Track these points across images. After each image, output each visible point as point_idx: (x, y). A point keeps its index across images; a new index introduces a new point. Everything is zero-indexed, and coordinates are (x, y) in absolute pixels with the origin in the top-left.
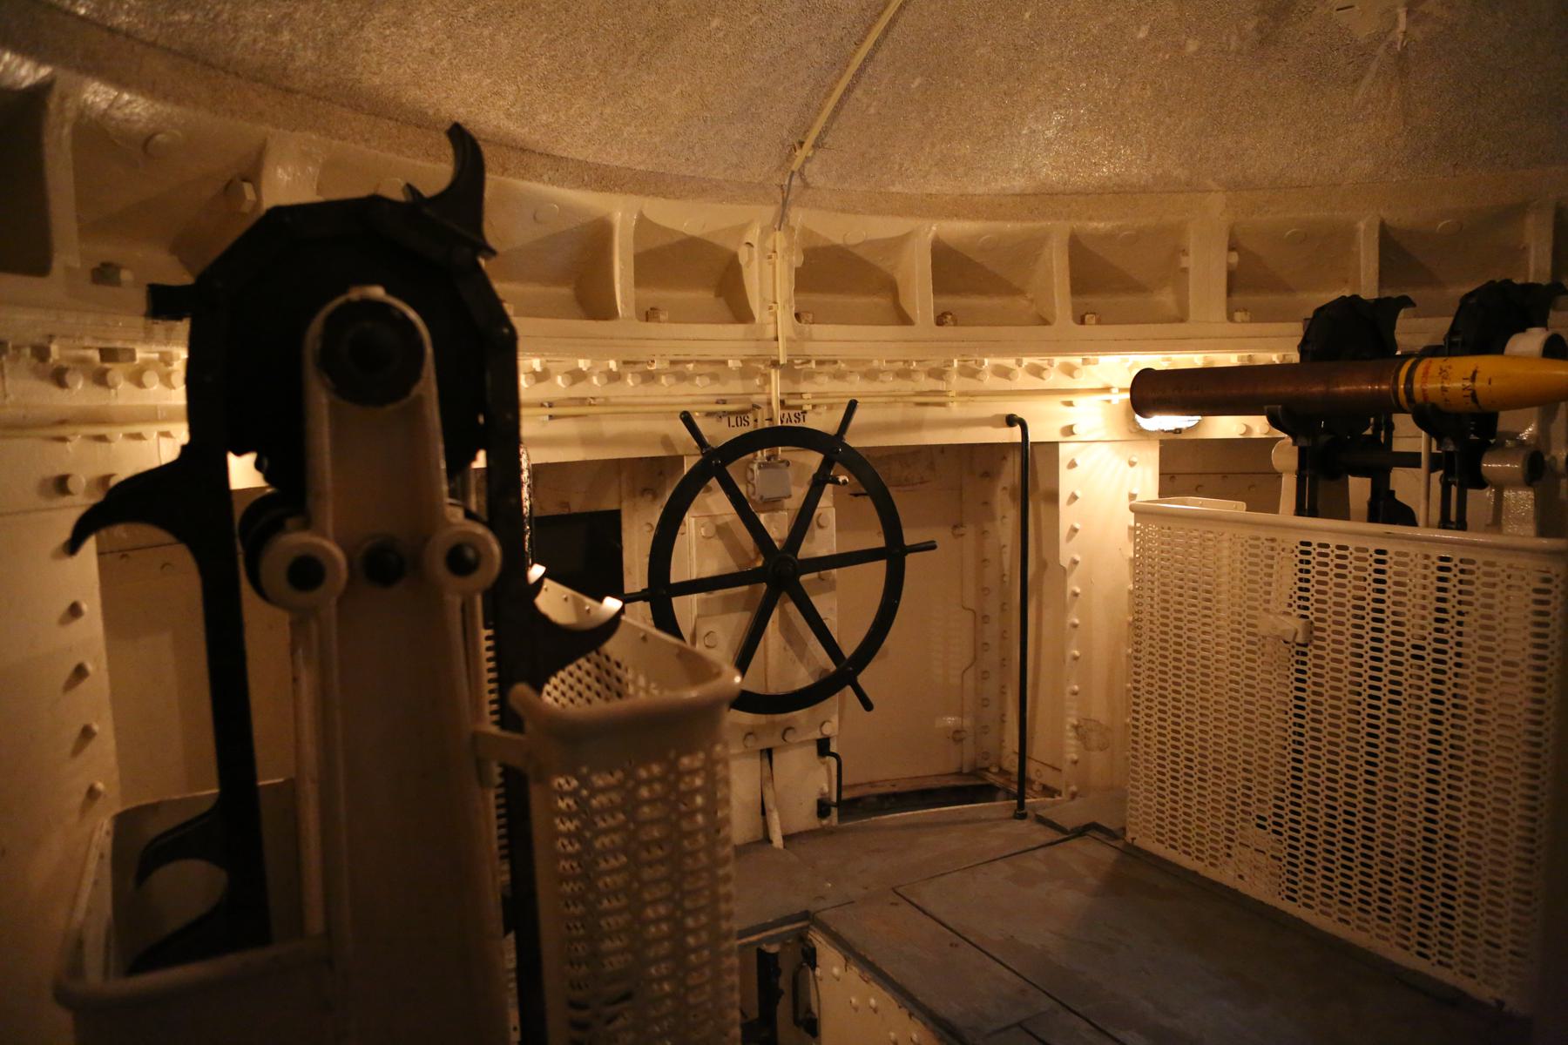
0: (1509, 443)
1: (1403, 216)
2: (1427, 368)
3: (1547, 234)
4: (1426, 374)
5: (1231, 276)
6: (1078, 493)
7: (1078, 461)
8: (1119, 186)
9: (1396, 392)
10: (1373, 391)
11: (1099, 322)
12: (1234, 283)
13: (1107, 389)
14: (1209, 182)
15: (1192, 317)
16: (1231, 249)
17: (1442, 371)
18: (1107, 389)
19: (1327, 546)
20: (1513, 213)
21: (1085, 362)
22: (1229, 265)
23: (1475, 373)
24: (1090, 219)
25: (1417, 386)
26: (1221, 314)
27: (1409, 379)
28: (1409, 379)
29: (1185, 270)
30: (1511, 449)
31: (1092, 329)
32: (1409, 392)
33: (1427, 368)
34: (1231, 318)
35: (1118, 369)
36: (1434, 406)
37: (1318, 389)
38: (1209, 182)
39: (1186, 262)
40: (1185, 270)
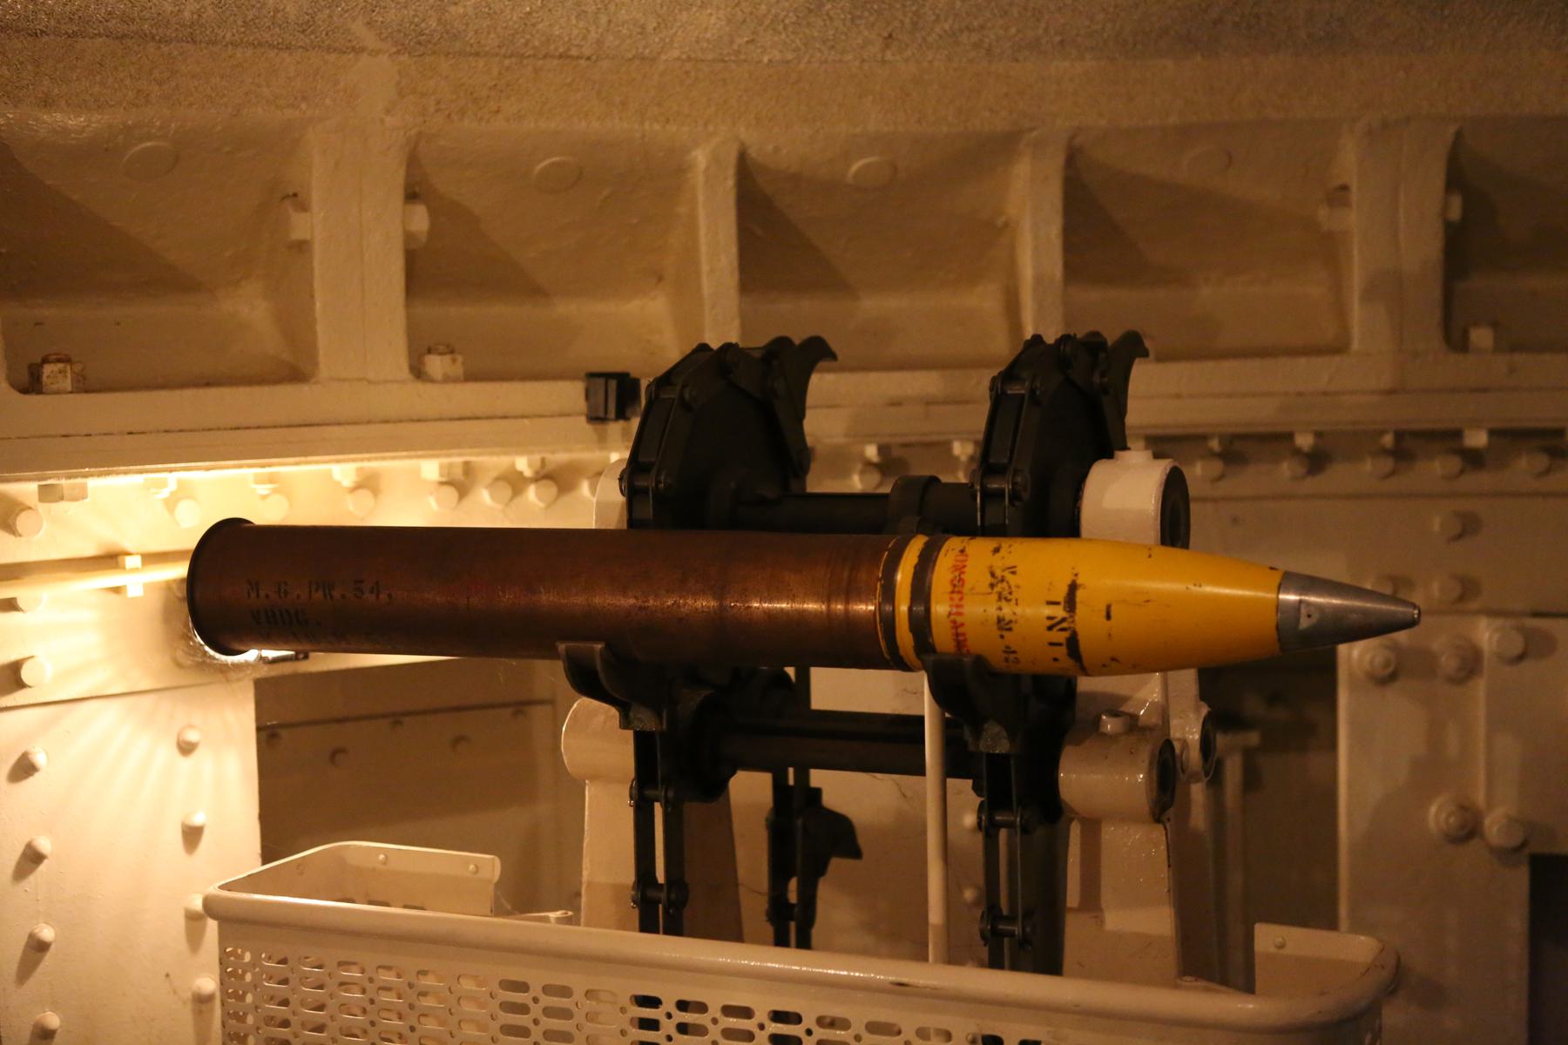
0: (1109, 725)
1: (786, 143)
2: (960, 569)
3: (1053, 194)
4: (957, 586)
5: (412, 260)
6: (44, 845)
7: (39, 759)
8: (126, 19)
9: (889, 622)
10: (830, 615)
11: (84, 386)
12: (424, 273)
13: (110, 559)
14: (358, 27)
15: (324, 371)
16: (411, 196)
17: (996, 580)
18: (110, 559)
19: (746, 1013)
20: (988, 153)
21: (47, 494)
22: (409, 237)
23: (1073, 588)
24: (47, 103)
25: (940, 608)
26: (397, 360)
27: (921, 591)
28: (921, 591)
29: (302, 247)
30: (1112, 738)
31: (62, 408)
32: (921, 624)
33: (960, 569)
34: (418, 372)
35: (154, 509)
36: (980, 661)
37: (706, 603)
38: (358, 27)
39: (301, 226)
40: (302, 247)
